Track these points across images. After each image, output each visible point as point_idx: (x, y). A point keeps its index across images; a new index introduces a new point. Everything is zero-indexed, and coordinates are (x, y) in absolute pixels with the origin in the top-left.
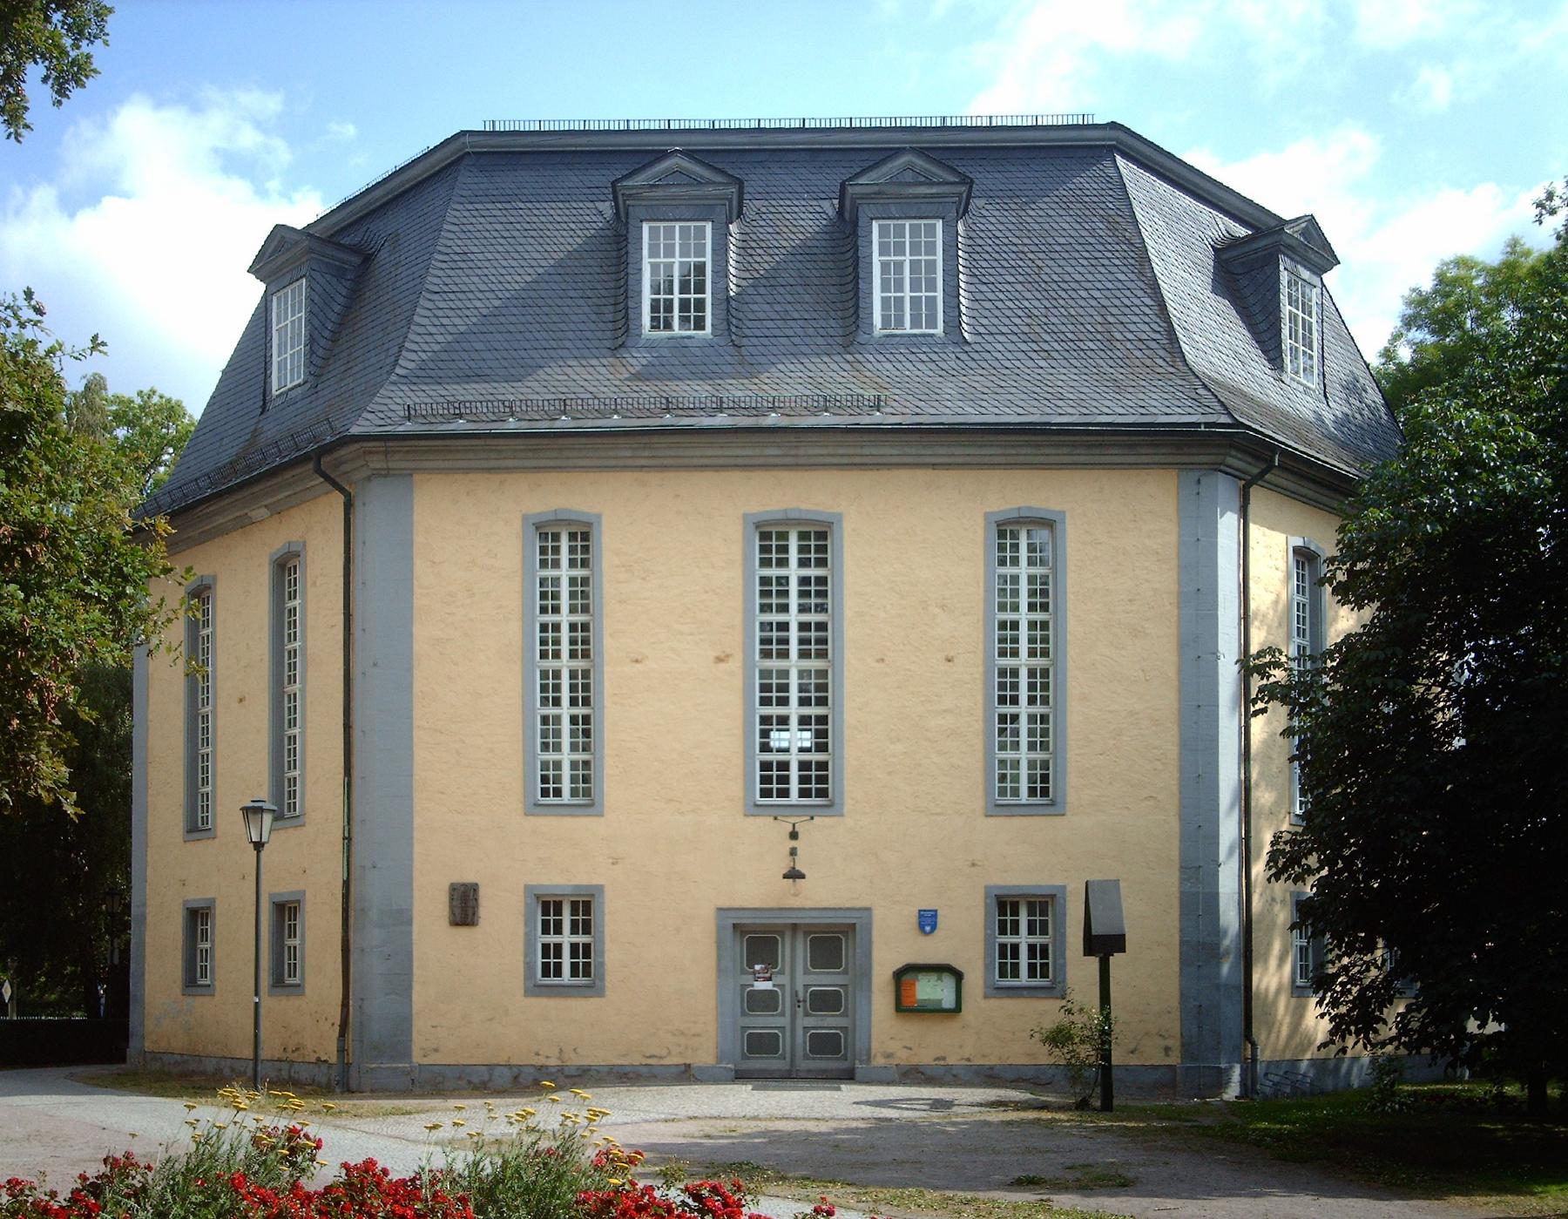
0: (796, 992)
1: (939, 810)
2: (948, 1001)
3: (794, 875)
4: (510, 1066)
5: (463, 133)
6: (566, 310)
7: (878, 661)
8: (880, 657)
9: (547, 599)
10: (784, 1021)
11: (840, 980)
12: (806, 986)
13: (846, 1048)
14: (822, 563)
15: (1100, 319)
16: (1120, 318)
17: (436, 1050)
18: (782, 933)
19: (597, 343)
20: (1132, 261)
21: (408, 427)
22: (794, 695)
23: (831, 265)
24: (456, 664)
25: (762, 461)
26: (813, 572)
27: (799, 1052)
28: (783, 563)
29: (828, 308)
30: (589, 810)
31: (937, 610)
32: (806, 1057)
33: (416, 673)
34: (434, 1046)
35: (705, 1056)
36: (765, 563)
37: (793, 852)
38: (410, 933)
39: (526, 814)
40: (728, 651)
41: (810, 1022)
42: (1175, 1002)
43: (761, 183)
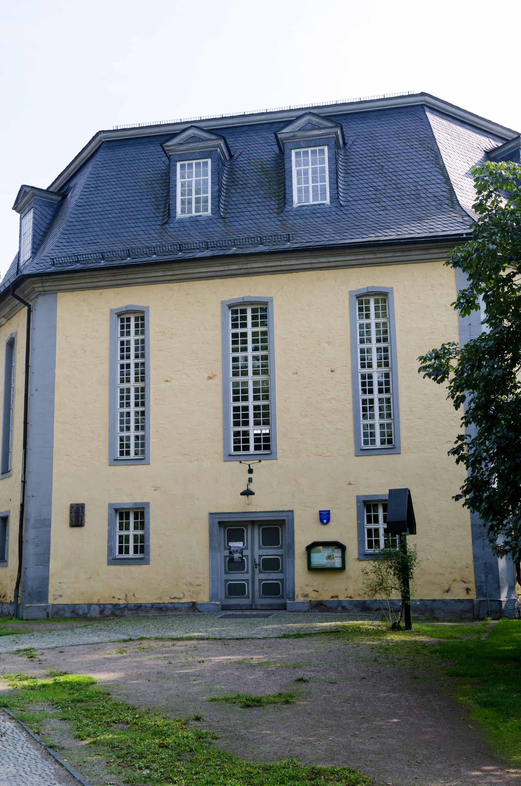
0: (255, 559)
1: (330, 454)
2: (338, 563)
3: (248, 493)
4: (99, 605)
5: (100, 132)
6: (141, 209)
7: (294, 374)
8: (295, 371)
9: (367, 339)
10: (248, 576)
11: (279, 552)
12: (260, 556)
13: (283, 591)
14: (264, 324)
15: (414, 188)
16: (424, 187)
17: (61, 596)
18: (246, 527)
19: (154, 223)
20: (432, 158)
21: (53, 269)
22: (251, 394)
23: (275, 175)
24: (76, 387)
25: (229, 273)
26: (259, 329)
27: (257, 594)
28: (244, 325)
29: (271, 196)
30: (143, 462)
31: (326, 345)
32: (260, 597)
33: (56, 393)
34: (60, 594)
35: (203, 598)
36: (235, 326)
37: (250, 480)
38: (49, 532)
39: (110, 465)
40: (215, 373)
41: (263, 576)
42: (470, 561)
43: (243, 141)
